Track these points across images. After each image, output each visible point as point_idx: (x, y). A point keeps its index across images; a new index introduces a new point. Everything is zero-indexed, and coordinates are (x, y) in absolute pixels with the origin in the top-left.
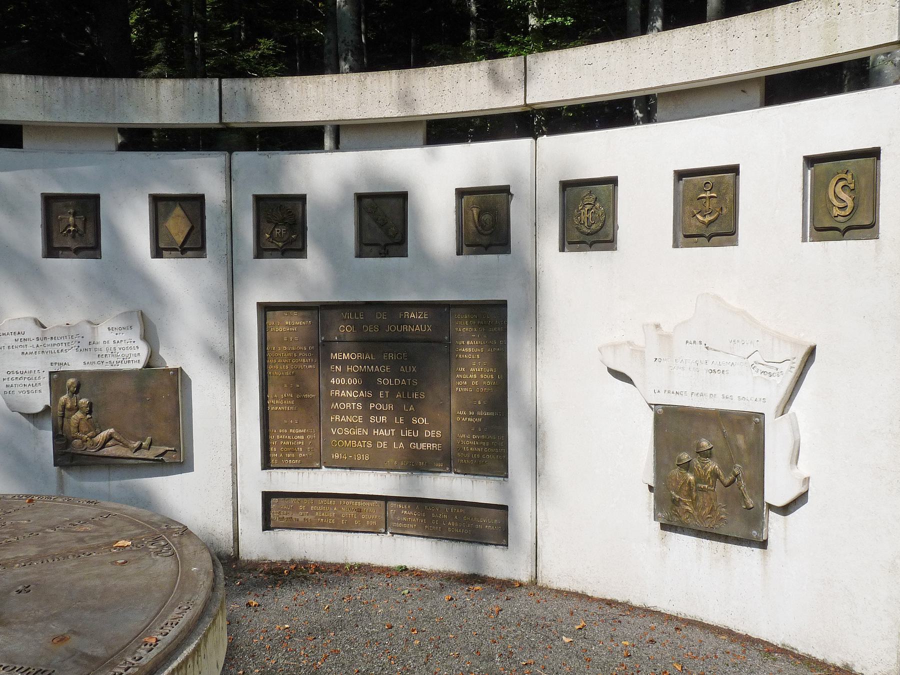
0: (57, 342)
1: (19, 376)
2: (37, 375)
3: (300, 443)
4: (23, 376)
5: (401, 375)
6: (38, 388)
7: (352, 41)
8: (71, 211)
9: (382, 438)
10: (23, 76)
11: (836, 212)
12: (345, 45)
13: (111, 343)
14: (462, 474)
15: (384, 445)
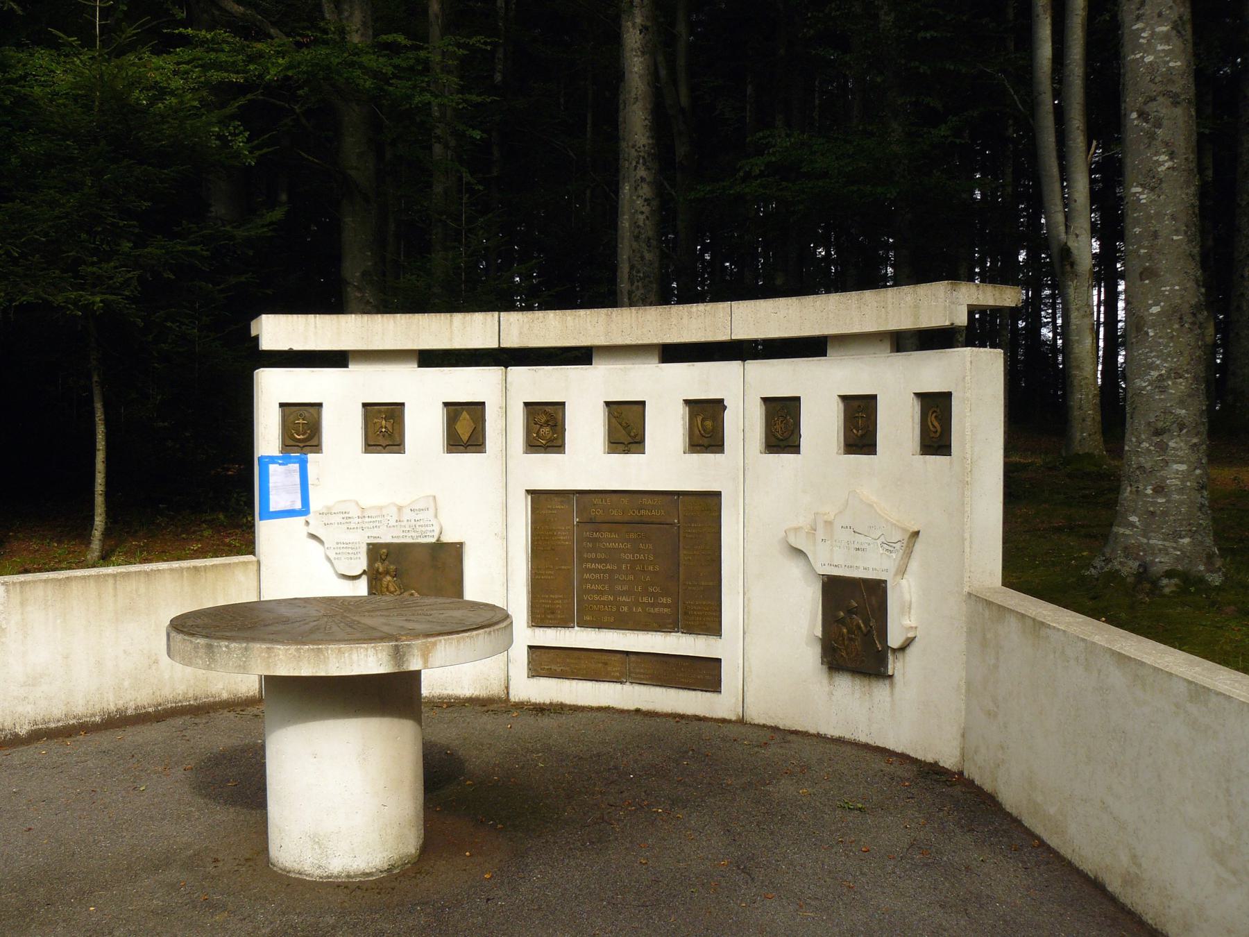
0: (373, 520)
1: (345, 546)
2: (357, 546)
3: (558, 606)
4: (347, 546)
5: (639, 551)
6: (359, 556)
7: (644, 146)
8: (384, 416)
9: (625, 604)
10: (353, 316)
11: (932, 435)
12: (636, 150)
13: (413, 521)
14: (688, 633)
15: (625, 609)
